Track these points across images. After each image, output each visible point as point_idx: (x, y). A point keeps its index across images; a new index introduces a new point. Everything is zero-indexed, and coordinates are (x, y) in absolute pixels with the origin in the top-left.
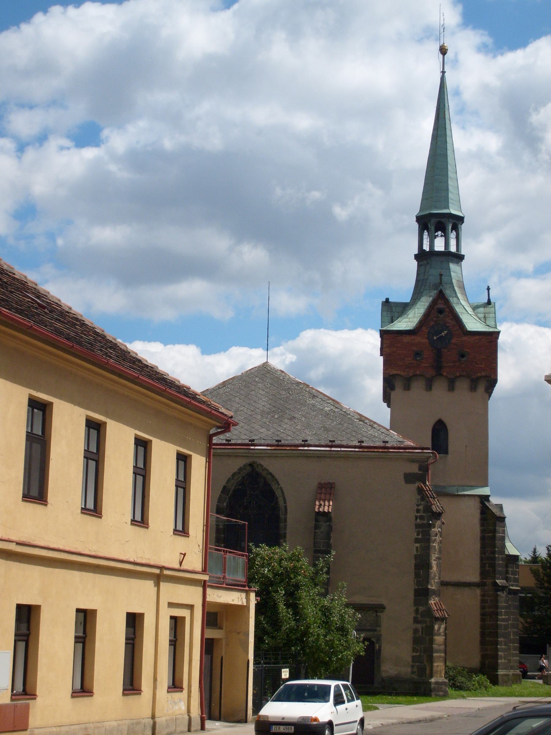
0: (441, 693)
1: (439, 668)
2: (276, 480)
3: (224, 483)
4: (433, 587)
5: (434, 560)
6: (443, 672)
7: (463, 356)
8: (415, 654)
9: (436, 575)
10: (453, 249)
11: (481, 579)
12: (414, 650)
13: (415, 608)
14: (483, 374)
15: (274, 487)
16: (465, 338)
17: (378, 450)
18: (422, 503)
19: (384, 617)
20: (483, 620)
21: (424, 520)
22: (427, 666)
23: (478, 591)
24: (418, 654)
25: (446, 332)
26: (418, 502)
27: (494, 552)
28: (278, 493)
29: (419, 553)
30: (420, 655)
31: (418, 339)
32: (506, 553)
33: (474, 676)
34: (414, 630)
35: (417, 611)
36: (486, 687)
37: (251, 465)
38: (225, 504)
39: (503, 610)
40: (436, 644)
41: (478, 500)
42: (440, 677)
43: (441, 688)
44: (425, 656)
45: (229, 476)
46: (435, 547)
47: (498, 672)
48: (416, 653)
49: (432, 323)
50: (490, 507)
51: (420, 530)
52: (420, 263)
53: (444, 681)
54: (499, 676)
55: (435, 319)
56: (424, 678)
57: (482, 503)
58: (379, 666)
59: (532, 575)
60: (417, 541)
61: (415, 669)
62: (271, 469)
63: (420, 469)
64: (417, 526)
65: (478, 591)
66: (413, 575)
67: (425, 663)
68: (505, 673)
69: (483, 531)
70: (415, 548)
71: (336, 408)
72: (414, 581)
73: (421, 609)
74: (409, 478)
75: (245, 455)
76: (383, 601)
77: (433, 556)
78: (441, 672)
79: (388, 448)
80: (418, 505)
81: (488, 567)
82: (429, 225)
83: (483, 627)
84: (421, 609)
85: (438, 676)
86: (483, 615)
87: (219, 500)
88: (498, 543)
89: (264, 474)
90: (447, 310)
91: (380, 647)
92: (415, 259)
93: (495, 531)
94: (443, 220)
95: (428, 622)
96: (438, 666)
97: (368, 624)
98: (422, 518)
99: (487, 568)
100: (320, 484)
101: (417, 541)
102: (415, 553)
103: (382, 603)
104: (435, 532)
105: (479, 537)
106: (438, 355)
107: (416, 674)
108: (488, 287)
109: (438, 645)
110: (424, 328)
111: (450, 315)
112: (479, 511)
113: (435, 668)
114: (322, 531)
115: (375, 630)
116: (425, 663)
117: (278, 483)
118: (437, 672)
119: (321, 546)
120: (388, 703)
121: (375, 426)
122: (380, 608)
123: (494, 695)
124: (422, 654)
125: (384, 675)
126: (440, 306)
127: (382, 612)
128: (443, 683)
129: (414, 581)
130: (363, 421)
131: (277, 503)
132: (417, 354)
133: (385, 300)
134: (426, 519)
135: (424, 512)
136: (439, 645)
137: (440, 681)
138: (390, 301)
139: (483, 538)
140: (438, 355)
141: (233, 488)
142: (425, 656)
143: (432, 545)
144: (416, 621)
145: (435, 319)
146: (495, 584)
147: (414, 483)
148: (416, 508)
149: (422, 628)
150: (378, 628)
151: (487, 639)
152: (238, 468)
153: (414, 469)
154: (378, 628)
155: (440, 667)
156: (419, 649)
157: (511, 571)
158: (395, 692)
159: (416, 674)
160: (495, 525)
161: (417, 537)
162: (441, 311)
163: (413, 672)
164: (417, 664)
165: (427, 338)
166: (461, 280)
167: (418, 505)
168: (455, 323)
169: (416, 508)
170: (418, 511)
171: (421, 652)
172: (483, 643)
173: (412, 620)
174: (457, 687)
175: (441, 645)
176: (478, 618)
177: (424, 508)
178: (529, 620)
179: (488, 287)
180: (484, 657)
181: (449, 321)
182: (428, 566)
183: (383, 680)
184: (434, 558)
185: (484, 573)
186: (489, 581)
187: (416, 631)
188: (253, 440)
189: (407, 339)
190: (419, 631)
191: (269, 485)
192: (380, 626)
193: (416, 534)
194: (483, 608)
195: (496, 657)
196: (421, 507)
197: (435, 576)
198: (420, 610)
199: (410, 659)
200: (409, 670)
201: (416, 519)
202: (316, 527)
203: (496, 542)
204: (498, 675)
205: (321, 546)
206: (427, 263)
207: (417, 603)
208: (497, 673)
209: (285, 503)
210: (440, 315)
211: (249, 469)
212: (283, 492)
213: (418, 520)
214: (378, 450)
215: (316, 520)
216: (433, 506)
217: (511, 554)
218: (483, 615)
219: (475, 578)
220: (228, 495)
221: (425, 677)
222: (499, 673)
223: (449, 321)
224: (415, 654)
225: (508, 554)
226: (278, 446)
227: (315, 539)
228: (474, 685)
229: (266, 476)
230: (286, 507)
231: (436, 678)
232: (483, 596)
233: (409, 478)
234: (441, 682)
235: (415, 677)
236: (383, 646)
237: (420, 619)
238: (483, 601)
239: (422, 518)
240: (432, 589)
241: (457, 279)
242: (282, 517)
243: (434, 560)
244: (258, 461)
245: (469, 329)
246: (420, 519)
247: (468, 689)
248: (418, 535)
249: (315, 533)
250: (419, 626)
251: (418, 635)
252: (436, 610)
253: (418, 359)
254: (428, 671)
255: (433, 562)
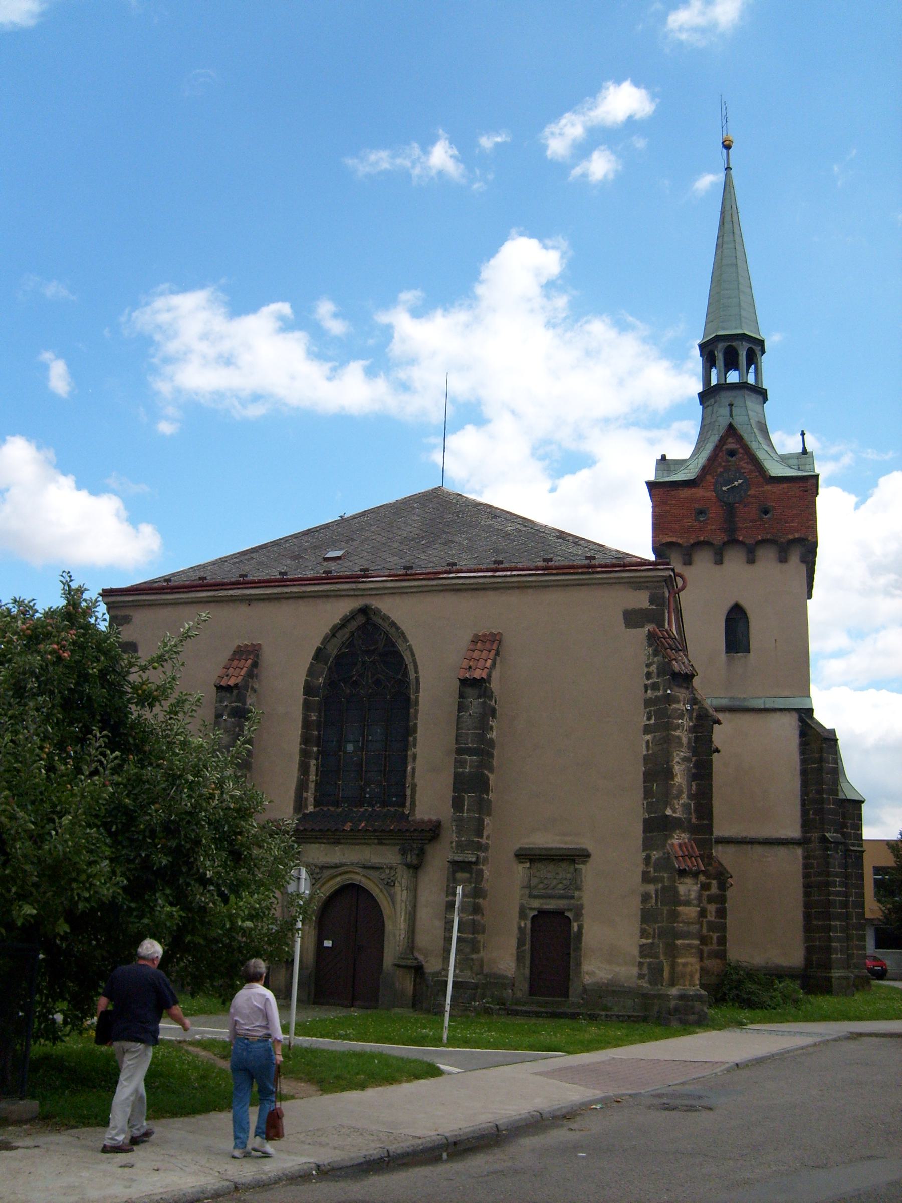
0: (692, 1017)
1: (689, 969)
2: (403, 633)
3: (317, 643)
4: (676, 813)
5: (678, 763)
6: (697, 976)
7: (766, 512)
8: (644, 941)
9: (682, 791)
10: (751, 380)
11: (803, 832)
12: (644, 934)
13: (644, 854)
14: (797, 536)
15: (401, 647)
16: (768, 487)
17: (576, 571)
18: (656, 659)
19: (588, 871)
20: (807, 894)
21: (659, 690)
22: (665, 964)
23: (799, 851)
24: (650, 941)
25: (740, 481)
26: (649, 659)
27: (820, 792)
28: (408, 659)
29: (651, 752)
30: (652, 943)
31: (699, 492)
32: (841, 796)
33: (777, 982)
34: (643, 896)
35: (648, 859)
36: (796, 1002)
37: (365, 610)
38: (321, 680)
39: (838, 879)
40: (681, 922)
41: (795, 716)
42: (690, 985)
43: (692, 1007)
44: (661, 945)
45: (326, 630)
46: (679, 738)
47: (831, 973)
48: (647, 938)
49: (720, 470)
50: (813, 726)
51: (653, 709)
52: (705, 405)
53: (698, 993)
54: (833, 980)
55: (723, 464)
56: (660, 987)
57: (801, 720)
58: (579, 965)
59: (890, 850)
60: (647, 730)
61: (645, 971)
62: (395, 616)
63: (652, 601)
64: (648, 703)
65: (799, 851)
66: (641, 794)
67: (662, 957)
68: (842, 974)
69: (803, 762)
70: (644, 743)
71: (525, 526)
72: (644, 804)
73: (656, 855)
74: (633, 618)
75: (352, 593)
76: (586, 843)
77: (675, 754)
78: (692, 976)
79: (594, 567)
80: (648, 665)
81: (813, 814)
82: (716, 352)
83: (807, 905)
84: (656, 855)
85: (687, 983)
86: (807, 887)
87: (311, 672)
88: (827, 777)
89: (386, 625)
90: (741, 450)
91: (580, 928)
92: (833, 732)
93: (821, 760)
94: (733, 344)
95: (666, 880)
96: (685, 965)
97: (560, 886)
98: (655, 686)
99: (811, 816)
100: (476, 635)
101: (647, 730)
102: (645, 753)
103: (584, 846)
104: (679, 712)
105: (798, 772)
106: (730, 511)
107: (647, 978)
108: (803, 431)
109: (685, 923)
110: (709, 478)
111: (746, 457)
112: (797, 732)
113: (679, 969)
114: (470, 715)
115: (572, 897)
116: (662, 957)
117: (406, 640)
118: (683, 976)
119: (469, 740)
120: (532, 1047)
121: (582, 543)
122: (583, 856)
123: (809, 1018)
124: (656, 941)
125: (587, 980)
126: (731, 445)
127: (584, 863)
128: (699, 998)
129: (644, 804)
130: (564, 539)
131: (406, 674)
132: (701, 512)
133: (660, 458)
134: (662, 688)
135: (659, 676)
136: (688, 923)
137: (691, 993)
138: (667, 458)
139: (804, 773)
140: (730, 511)
141: (335, 652)
142: (661, 945)
143: (673, 736)
144: (646, 878)
145: (723, 464)
146: (824, 839)
147: (643, 626)
148: (646, 672)
149: (657, 891)
150: (577, 894)
151: (815, 923)
152: (341, 617)
153: (641, 600)
154: (577, 894)
155: (689, 966)
156: (651, 931)
157: (851, 823)
158: (604, 1013)
159: (647, 978)
160: (821, 750)
161: (648, 723)
162: (732, 453)
163: (641, 976)
164: (648, 960)
165: (714, 491)
166: (763, 422)
167: (648, 665)
168: (753, 468)
169: (646, 670)
170: (649, 675)
171: (654, 937)
172: (808, 929)
173: (638, 878)
174: (743, 1001)
175: (692, 923)
176: (800, 890)
177: (658, 669)
178: (889, 906)
179: (803, 431)
180: (809, 951)
181: (745, 465)
182: (669, 774)
183: (585, 990)
184: (677, 759)
185: (806, 824)
186: (815, 835)
187: (646, 898)
188: (367, 570)
189: (685, 493)
190: (651, 898)
191: (394, 645)
192: (579, 888)
193: (645, 718)
194: (806, 876)
195: (829, 950)
196: (654, 668)
197: (680, 792)
198: (654, 858)
199: (636, 952)
200: (635, 971)
201: (646, 691)
202: (461, 708)
203: (825, 776)
204: (832, 977)
205: (469, 740)
206: (715, 402)
207: (648, 845)
208: (830, 975)
209: (417, 672)
210: (730, 459)
211: (361, 619)
212: (413, 655)
213: (649, 691)
214: (576, 571)
215: (461, 695)
216: (674, 662)
217: (849, 798)
218: (808, 887)
219: (793, 831)
220: (326, 664)
221: (662, 986)
222: (833, 975)
223: (745, 465)
224: (644, 941)
225: (844, 798)
226: (407, 575)
227: (458, 729)
228: (772, 998)
229: (388, 628)
230: (417, 679)
231: (681, 988)
232: (806, 857)
233: (633, 618)
234: (690, 996)
235: (645, 985)
236: (585, 926)
237: (653, 874)
238: (806, 866)
239: (655, 686)
240: (674, 817)
241: (757, 420)
242: (413, 697)
243: (678, 763)
244: (374, 602)
245: (773, 475)
246: (652, 690)
247: (761, 1006)
248: (649, 719)
249: (459, 717)
250: (651, 888)
251: (649, 906)
252: (682, 856)
253: (701, 519)
254: (666, 975)
255: (676, 767)
